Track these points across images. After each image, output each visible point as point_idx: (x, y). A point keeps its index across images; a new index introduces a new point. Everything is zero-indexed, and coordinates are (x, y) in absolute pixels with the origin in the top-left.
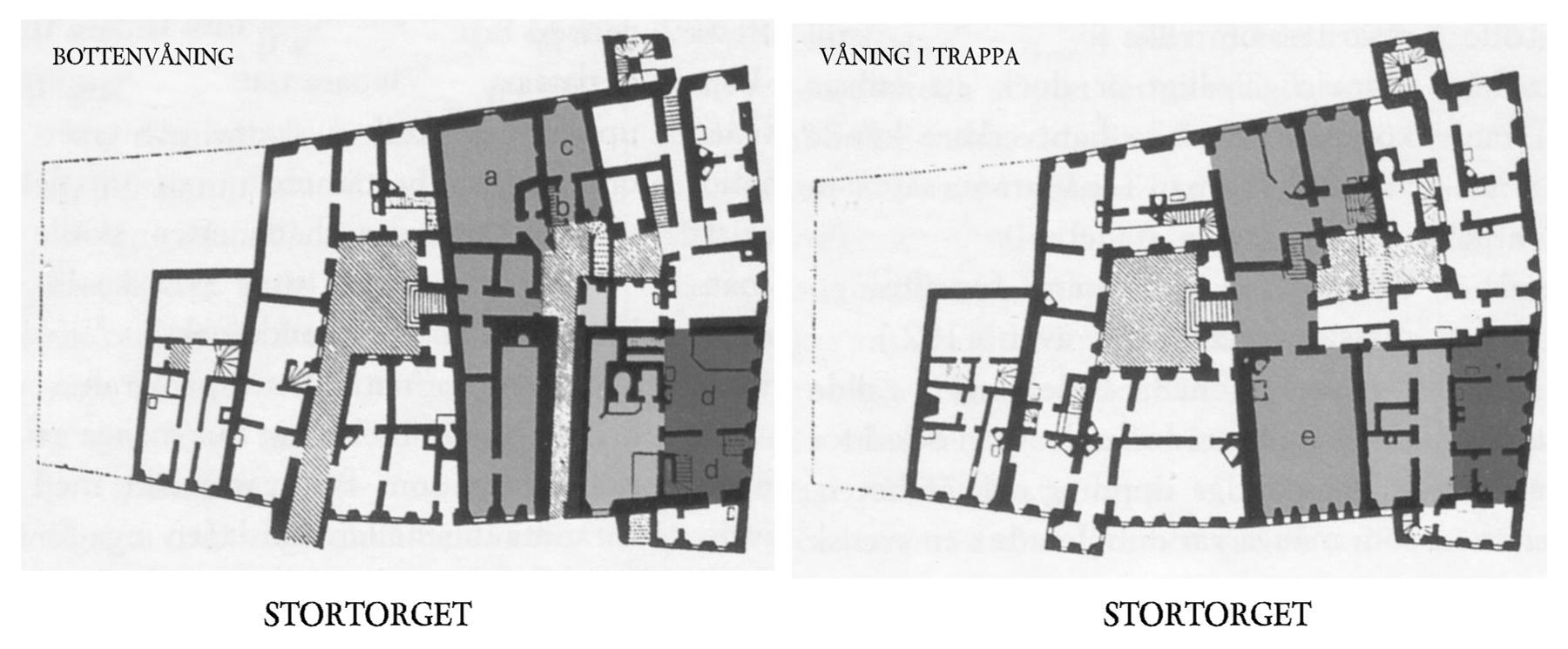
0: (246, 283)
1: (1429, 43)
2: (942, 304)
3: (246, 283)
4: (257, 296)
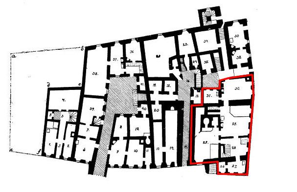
0: (79, 91)
2: (51, 91)
4: (83, 96)
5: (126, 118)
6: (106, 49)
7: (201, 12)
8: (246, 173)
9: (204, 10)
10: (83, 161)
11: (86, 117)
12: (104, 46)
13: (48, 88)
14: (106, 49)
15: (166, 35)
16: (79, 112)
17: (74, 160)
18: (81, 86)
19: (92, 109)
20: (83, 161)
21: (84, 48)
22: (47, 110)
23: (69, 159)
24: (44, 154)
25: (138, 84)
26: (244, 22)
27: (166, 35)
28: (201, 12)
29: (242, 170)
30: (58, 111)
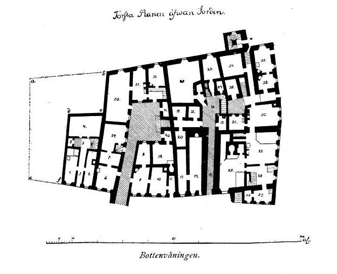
0: (101, 117)
1: (243, 34)
3: (101, 117)
5: (149, 145)
6: (129, 74)
7: (226, 35)
8: (273, 202)
9: (230, 34)
10: (104, 190)
11: (108, 145)
12: (126, 70)
13: (69, 114)
14: (129, 74)
15: (191, 59)
16: (101, 138)
17: (96, 189)
18: (102, 112)
19: (114, 136)
20: (104, 190)
21: (106, 73)
22: (68, 137)
23: (90, 188)
24: (64, 183)
25: (161, 109)
26: (270, 46)
27: (191, 59)
28: (226, 35)
29: (268, 198)
30: (78, 137)
